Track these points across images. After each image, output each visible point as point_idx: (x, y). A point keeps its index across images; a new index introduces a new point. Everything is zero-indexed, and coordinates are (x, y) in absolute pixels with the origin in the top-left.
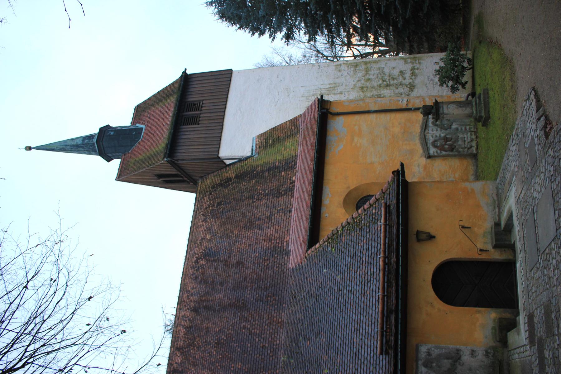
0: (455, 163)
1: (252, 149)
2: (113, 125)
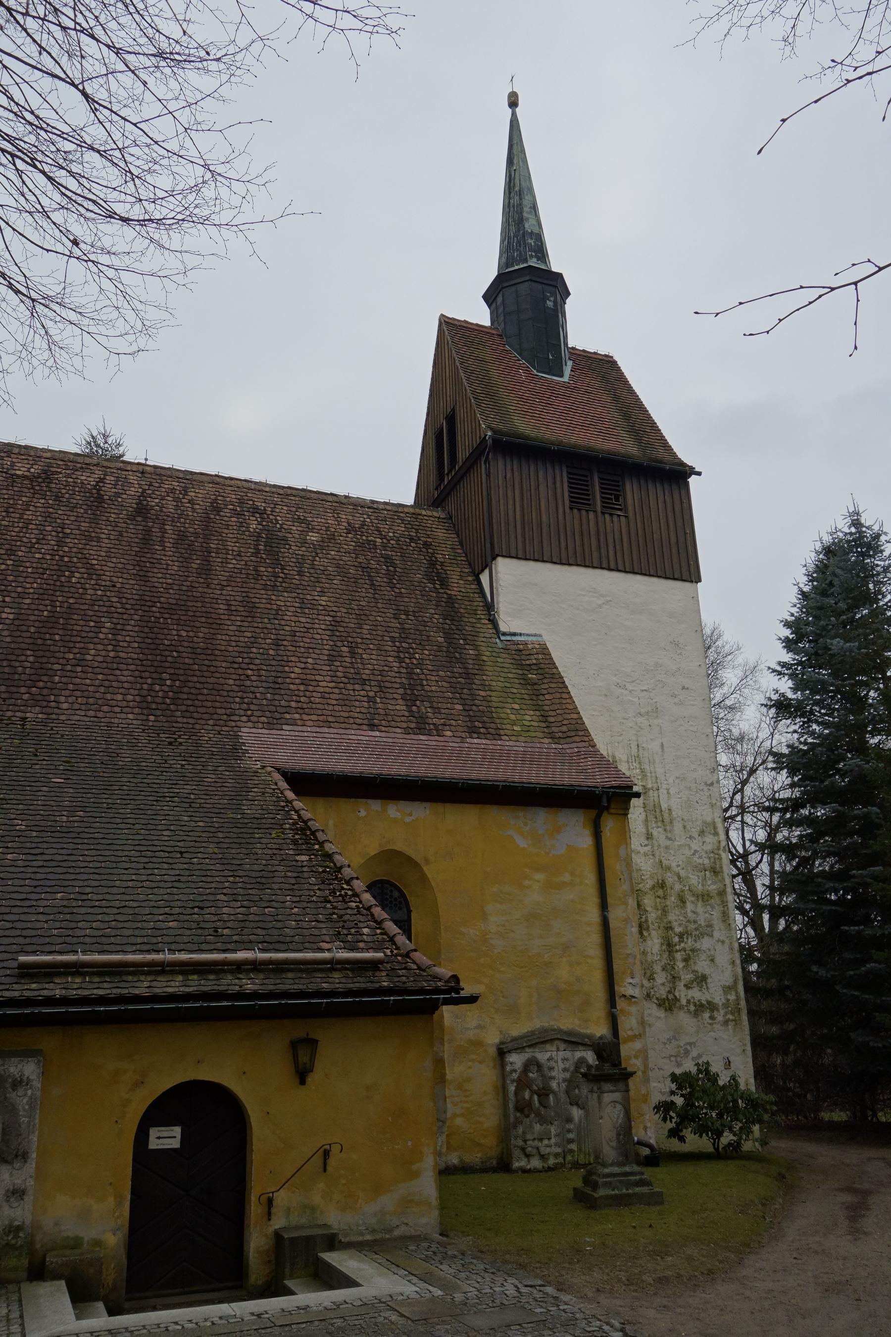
0: (490, 1118)
1: (514, 634)
2: (570, 306)
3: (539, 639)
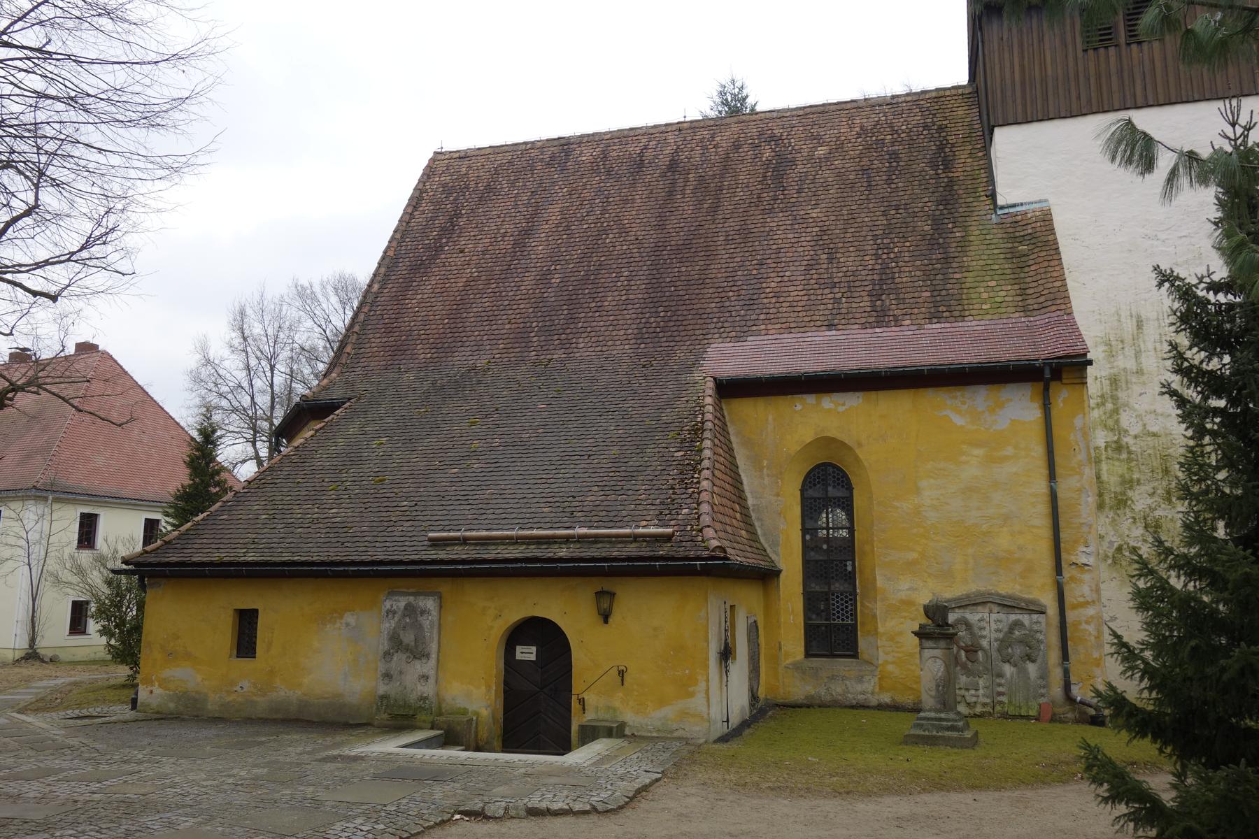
1: (1014, 206)
3: (1044, 205)
